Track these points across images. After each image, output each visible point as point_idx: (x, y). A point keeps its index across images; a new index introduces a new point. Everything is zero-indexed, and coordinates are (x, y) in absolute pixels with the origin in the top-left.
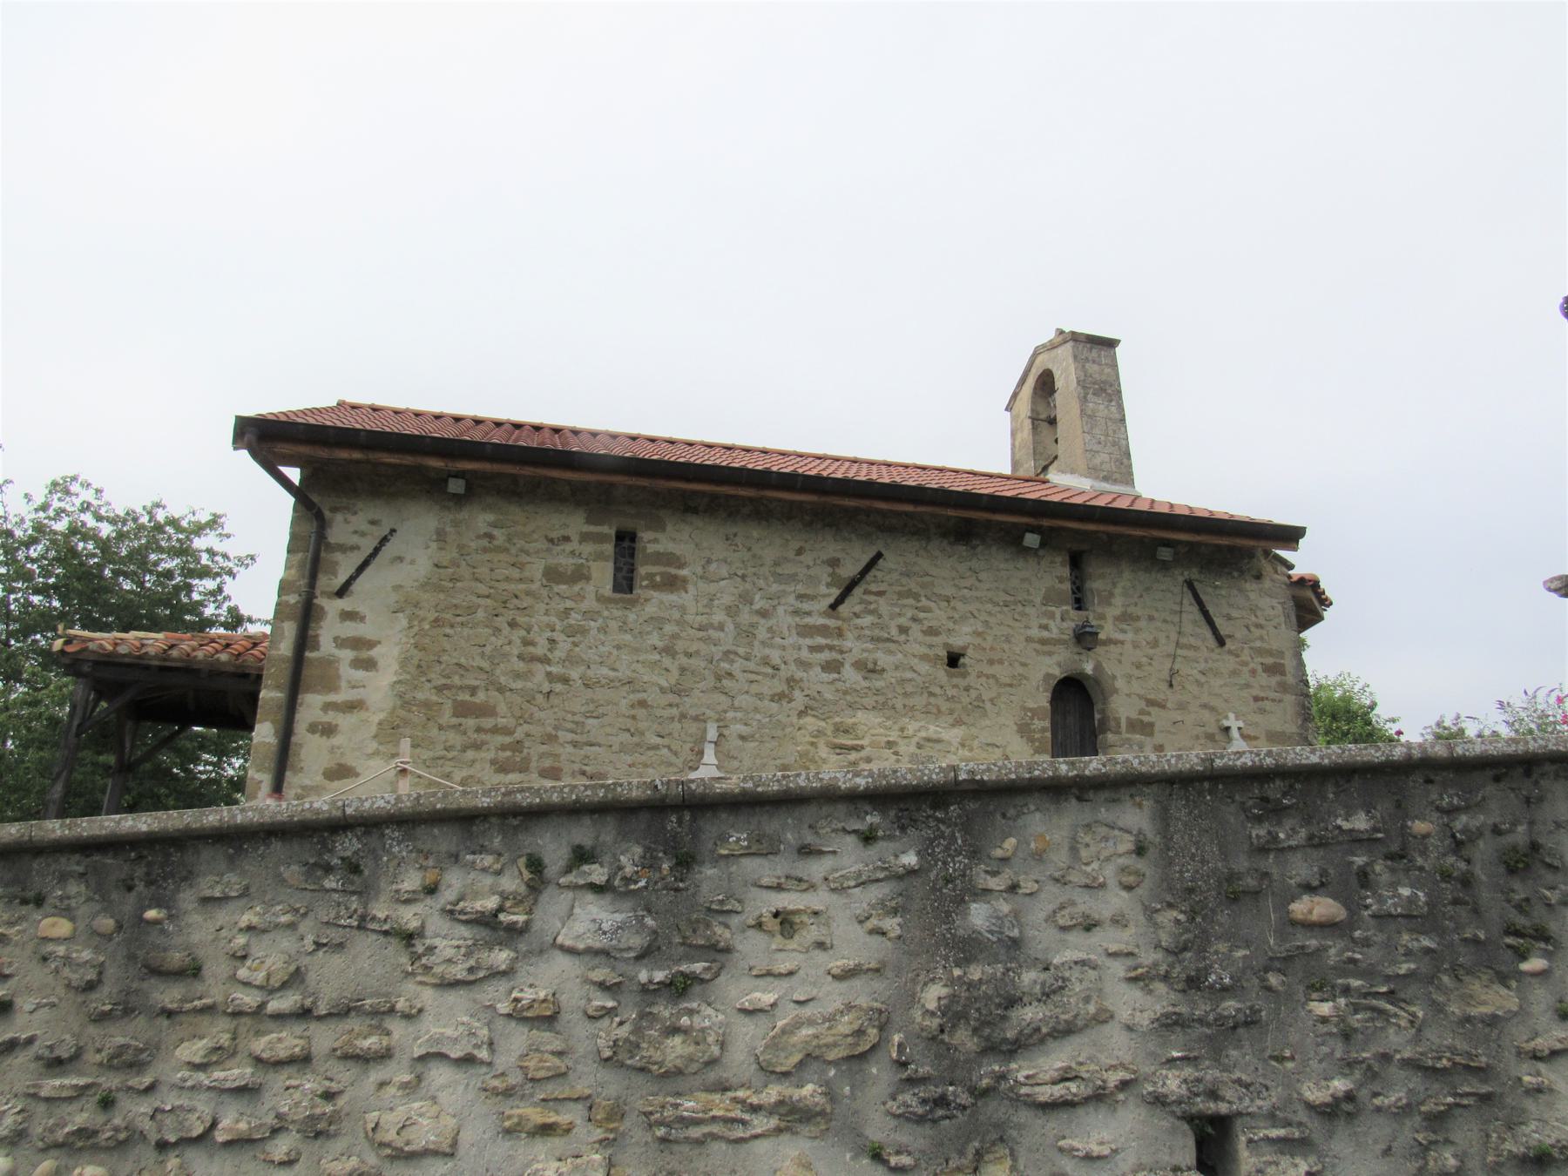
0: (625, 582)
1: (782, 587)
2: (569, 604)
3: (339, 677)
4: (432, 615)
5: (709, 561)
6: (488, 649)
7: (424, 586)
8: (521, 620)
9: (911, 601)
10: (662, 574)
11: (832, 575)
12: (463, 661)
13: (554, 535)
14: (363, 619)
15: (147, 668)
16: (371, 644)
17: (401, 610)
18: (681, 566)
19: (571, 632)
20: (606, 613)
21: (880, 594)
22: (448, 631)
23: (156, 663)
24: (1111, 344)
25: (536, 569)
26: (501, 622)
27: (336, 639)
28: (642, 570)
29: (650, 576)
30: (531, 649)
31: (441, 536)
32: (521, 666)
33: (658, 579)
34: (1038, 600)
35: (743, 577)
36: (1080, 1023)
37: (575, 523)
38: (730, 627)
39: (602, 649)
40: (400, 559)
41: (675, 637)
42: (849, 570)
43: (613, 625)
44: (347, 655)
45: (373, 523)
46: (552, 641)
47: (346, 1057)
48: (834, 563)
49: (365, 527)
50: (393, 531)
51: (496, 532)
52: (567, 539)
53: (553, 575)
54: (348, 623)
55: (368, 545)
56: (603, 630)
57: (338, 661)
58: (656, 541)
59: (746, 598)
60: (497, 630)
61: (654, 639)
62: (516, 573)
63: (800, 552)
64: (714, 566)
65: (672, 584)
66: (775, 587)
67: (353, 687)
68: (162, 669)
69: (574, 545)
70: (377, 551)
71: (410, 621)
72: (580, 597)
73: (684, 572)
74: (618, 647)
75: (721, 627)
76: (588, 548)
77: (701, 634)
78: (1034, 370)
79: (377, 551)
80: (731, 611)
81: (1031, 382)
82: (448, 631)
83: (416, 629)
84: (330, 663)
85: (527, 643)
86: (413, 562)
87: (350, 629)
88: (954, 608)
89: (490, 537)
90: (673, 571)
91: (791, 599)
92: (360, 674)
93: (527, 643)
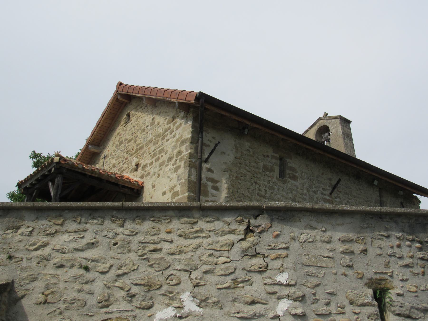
0: (282, 174)
1: (319, 185)
2: (270, 179)
3: (208, 192)
4: (235, 175)
5: (302, 172)
6: (250, 190)
7: (233, 164)
8: (258, 182)
9: (347, 196)
10: (292, 174)
11: (330, 183)
12: (244, 193)
13: (265, 154)
14: (213, 172)
15: (85, 175)
16: (217, 182)
17: (227, 171)
18: (296, 172)
19: (271, 188)
20: (279, 184)
21: (340, 192)
22: (240, 181)
23: (89, 174)
24: (349, 122)
25: (261, 165)
26: (253, 181)
27: (206, 177)
28: (288, 171)
29: (289, 174)
30: (261, 192)
31: (236, 148)
32: (258, 197)
33: (291, 175)
34: (374, 201)
35: (310, 179)
36: (184, 316)
37: (270, 151)
38: (308, 195)
39: (278, 196)
40: (224, 153)
41: (295, 195)
42: (334, 182)
43: (281, 189)
44: (210, 184)
45: (214, 138)
46: (266, 191)
47: (139, 308)
48: (330, 179)
49: (211, 139)
50: (219, 142)
51: (250, 150)
52: (268, 156)
53: (265, 168)
54: (209, 173)
55: (212, 146)
56: (278, 189)
57: (207, 185)
58: (290, 162)
59: (311, 186)
60: (252, 184)
61: (290, 196)
62: (255, 165)
63: (323, 174)
64: (303, 174)
65: (294, 178)
66: (317, 185)
67: (213, 196)
68: (91, 177)
69: (270, 159)
70: (215, 148)
71: (229, 176)
72: (272, 177)
73: (297, 174)
74: (282, 196)
75: (306, 195)
76: (274, 161)
77: (301, 196)
78: (318, 124)
79: (215, 148)
80: (308, 191)
81: (316, 128)
82: (240, 181)
83: (231, 179)
84: (206, 186)
85: (260, 190)
86: (228, 155)
87: (210, 175)
88: (356, 200)
89: (249, 150)
90: (295, 174)
91: (321, 189)
92: (214, 192)
93: (260, 190)
